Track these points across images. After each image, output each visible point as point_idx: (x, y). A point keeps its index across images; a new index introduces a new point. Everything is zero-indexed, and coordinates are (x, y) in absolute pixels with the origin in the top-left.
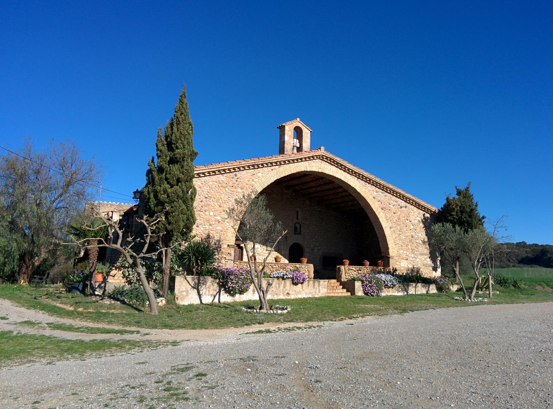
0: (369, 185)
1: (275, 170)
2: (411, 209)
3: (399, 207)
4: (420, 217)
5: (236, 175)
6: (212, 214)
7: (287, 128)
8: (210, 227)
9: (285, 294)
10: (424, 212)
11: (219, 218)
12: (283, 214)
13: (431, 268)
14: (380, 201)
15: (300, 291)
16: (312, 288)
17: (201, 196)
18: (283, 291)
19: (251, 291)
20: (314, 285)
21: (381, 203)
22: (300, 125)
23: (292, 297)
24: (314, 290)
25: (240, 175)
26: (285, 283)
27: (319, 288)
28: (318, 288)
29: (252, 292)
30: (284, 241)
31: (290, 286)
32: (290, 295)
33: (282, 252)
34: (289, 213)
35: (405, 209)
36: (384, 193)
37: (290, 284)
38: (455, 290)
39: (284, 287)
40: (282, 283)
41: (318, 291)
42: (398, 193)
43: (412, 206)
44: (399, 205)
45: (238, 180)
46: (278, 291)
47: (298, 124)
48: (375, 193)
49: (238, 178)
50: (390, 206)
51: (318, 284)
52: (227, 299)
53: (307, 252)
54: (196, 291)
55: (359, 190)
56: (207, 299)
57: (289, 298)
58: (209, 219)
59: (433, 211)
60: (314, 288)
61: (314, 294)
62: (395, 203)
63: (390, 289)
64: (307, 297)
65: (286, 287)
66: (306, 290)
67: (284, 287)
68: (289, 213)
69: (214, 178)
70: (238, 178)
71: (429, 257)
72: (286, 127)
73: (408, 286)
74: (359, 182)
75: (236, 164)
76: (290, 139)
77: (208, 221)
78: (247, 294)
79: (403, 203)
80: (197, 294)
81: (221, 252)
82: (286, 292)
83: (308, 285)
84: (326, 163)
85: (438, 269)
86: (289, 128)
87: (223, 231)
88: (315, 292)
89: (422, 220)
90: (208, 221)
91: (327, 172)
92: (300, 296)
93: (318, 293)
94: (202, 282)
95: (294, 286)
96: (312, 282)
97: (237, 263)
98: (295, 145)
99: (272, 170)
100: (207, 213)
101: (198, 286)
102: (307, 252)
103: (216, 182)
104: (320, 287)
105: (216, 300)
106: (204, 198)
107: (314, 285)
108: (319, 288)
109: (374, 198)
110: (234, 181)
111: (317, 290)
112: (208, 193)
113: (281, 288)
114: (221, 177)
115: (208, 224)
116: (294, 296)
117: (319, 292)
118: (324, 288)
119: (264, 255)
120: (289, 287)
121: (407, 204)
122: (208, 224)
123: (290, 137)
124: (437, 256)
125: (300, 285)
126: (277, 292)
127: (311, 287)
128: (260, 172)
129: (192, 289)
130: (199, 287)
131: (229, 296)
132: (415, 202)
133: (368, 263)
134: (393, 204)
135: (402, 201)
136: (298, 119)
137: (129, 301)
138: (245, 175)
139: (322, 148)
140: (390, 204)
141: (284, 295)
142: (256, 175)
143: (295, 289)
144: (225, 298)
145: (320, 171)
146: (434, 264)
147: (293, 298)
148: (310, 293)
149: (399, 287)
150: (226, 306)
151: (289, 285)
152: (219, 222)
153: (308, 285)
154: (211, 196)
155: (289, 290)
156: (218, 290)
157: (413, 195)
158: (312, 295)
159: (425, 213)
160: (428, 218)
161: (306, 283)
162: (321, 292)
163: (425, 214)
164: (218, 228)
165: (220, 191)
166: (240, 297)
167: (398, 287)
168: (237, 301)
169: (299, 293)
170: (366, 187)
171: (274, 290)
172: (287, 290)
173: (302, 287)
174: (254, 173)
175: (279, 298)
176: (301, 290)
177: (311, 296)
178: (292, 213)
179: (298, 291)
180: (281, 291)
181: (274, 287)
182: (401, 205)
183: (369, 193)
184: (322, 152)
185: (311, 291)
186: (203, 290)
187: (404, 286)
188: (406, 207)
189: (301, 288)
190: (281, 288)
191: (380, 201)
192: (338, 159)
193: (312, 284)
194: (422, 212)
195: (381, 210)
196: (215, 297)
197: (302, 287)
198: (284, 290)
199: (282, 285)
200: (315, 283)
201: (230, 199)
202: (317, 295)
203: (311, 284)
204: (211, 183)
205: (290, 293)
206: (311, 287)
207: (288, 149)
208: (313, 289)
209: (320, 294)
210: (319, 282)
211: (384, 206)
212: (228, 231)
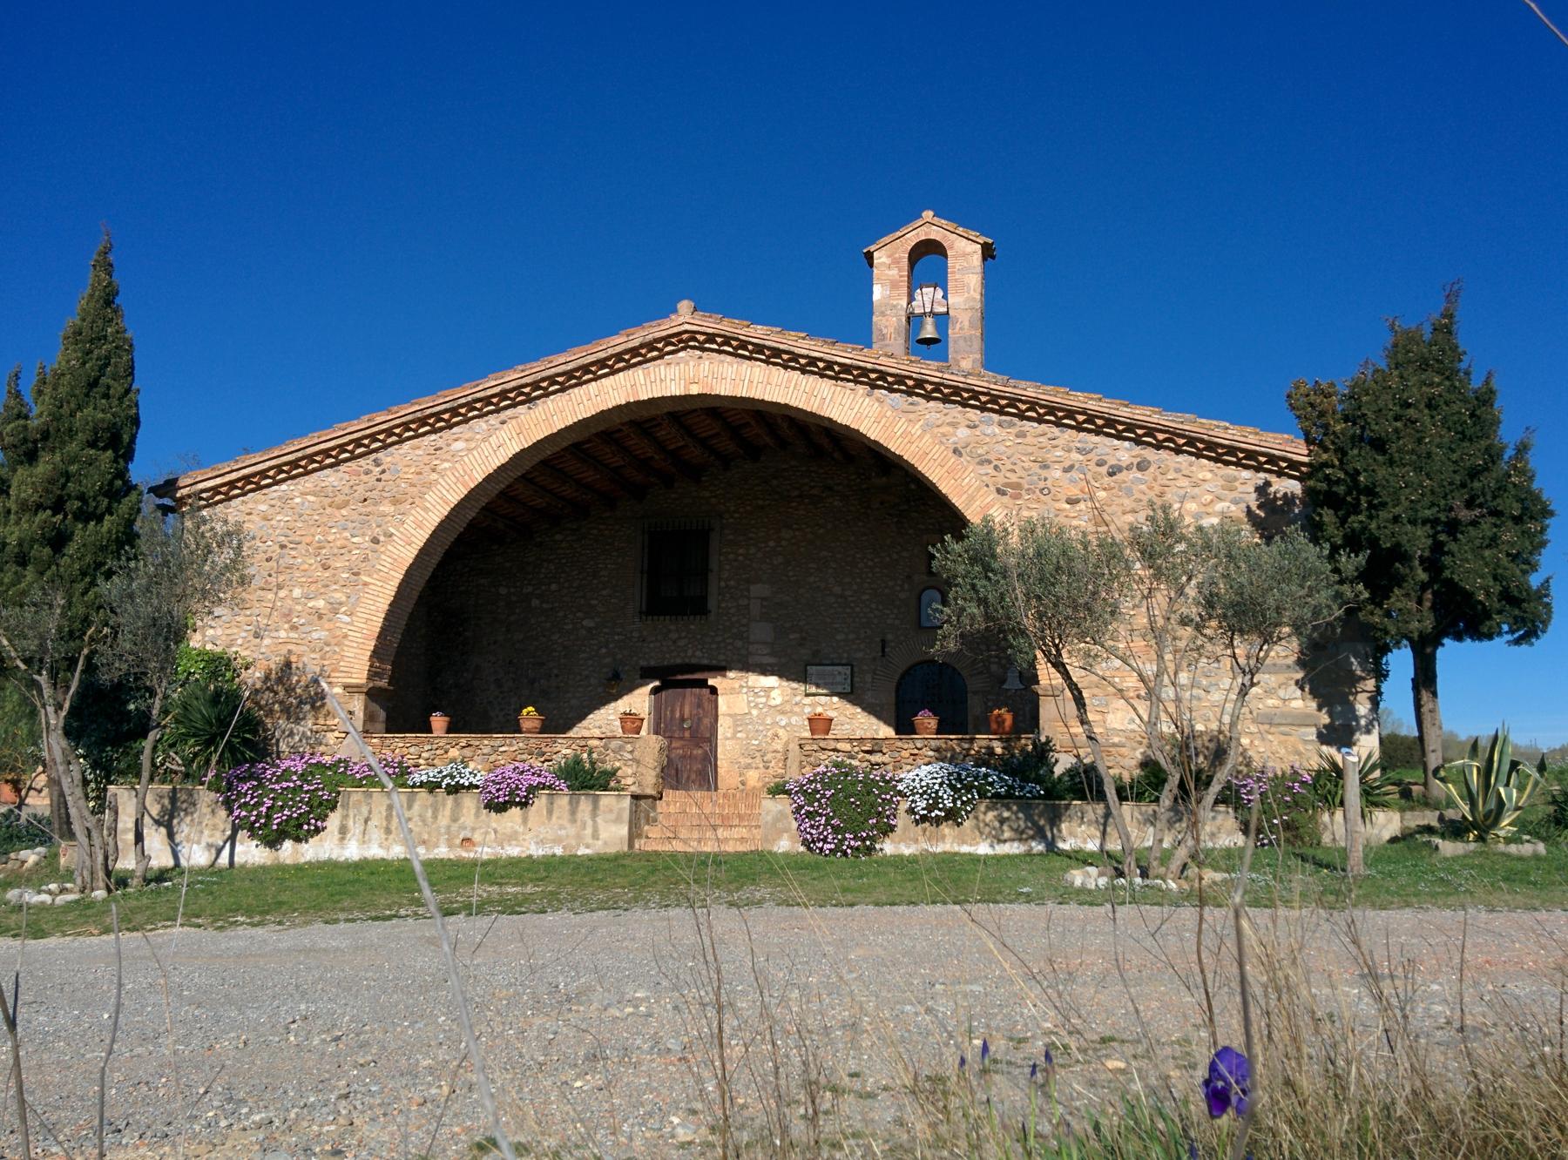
0: (932, 404)
1: (514, 421)
2: (1177, 470)
3: (1104, 470)
4: (1235, 502)
5: (377, 463)
6: (297, 592)
7: (880, 258)
8: (293, 635)
9: (458, 841)
10: (1262, 475)
11: (321, 603)
12: (870, 563)
13: (1311, 733)
14: (990, 462)
15: (516, 832)
16: (565, 822)
17: (270, 543)
18: (448, 832)
19: (332, 832)
20: (573, 812)
21: (996, 468)
22: (935, 234)
23: (485, 853)
24: (572, 830)
25: (389, 459)
26: (457, 804)
27: (595, 822)
28: (590, 823)
29: (337, 835)
30: (874, 659)
31: (477, 815)
32: (474, 845)
33: (869, 697)
34: (895, 556)
35: (1139, 475)
36: (1012, 425)
37: (478, 809)
38: (1387, 836)
39: (455, 819)
40: (444, 805)
41: (589, 831)
42: (1080, 413)
43: (1182, 458)
44: (1100, 464)
45: (384, 477)
46: (429, 833)
47: (926, 234)
48: (963, 433)
49: (383, 472)
50: (1044, 473)
51: (590, 808)
52: (254, 856)
53: (975, 693)
54: (163, 830)
55: (873, 433)
56: (197, 856)
57: (472, 855)
58: (290, 610)
59: (1303, 464)
60: (573, 821)
61: (574, 843)
62: (1075, 456)
63: (946, 829)
64: (541, 853)
65: (462, 820)
66: (542, 829)
67: (455, 819)
68: (895, 556)
69: (307, 483)
70: (383, 472)
71: (1300, 685)
72: (876, 255)
73: (1055, 818)
74: (878, 400)
75: (358, 426)
76: (895, 293)
77: (287, 615)
78: (321, 840)
79: (1125, 452)
80: (166, 838)
81: (324, 711)
82: (461, 837)
83: (550, 812)
84: (722, 357)
85: (1357, 736)
86: (889, 257)
87: (333, 641)
88: (579, 837)
89: (1249, 512)
90: (287, 615)
91: (724, 389)
92: (514, 851)
93: (590, 841)
94: (184, 806)
95: (493, 814)
96: (566, 799)
97: (374, 740)
98: (928, 310)
99: (503, 423)
100: (282, 594)
101: (172, 817)
102: (975, 693)
103: (314, 494)
104: (599, 820)
105: (224, 859)
106: (276, 547)
107: (573, 812)
108: (595, 822)
109: (955, 451)
110: (371, 479)
111: (584, 828)
112: (290, 533)
113: (444, 820)
114: (330, 478)
115: (286, 626)
116: (489, 850)
117: (595, 836)
118: (618, 820)
119: (796, 709)
120: (472, 817)
121: (1150, 454)
122: (286, 626)
123: (894, 285)
124: (1352, 672)
125: (515, 812)
126: (426, 837)
127: (559, 818)
128: (458, 440)
129: (155, 827)
130: (175, 821)
131: (261, 848)
132: (1183, 436)
133: (932, 723)
134: (1067, 464)
135: (1116, 442)
136: (928, 215)
137: (1156, 859)
138: (405, 457)
139: (685, 306)
140: (1046, 467)
141: (450, 846)
142: (445, 449)
143: (494, 825)
144: (250, 852)
145: (694, 390)
146: (1330, 714)
147: (485, 857)
148: (557, 841)
149: (1002, 821)
150: (257, 874)
151: (473, 811)
152: (320, 617)
153: (550, 812)
154: (297, 539)
155: (473, 829)
156: (229, 833)
157: (1167, 406)
158: (564, 848)
159: (1273, 478)
160: (1289, 499)
161: (540, 802)
162: (603, 835)
163: (1268, 484)
164: (315, 635)
165: (325, 520)
166: (296, 851)
167: (997, 824)
168: (288, 862)
169: (513, 837)
170: (911, 416)
171: (416, 829)
172: (465, 828)
173: (525, 820)
174: (440, 443)
175: (431, 856)
176: (521, 830)
177: (559, 851)
178: (905, 554)
179: (508, 831)
180: (443, 830)
181: (416, 819)
182: (1112, 462)
183: (927, 437)
184: (681, 320)
185: (563, 832)
186: (184, 829)
187: (1029, 818)
188: (1142, 466)
189: (519, 820)
190: (444, 820)
191: (990, 462)
192: (757, 333)
193: (567, 807)
194: (1246, 474)
195: (994, 495)
196: (219, 851)
197: (525, 820)
198: (455, 827)
199: (447, 812)
200: (578, 802)
201: (355, 540)
202: (588, 847)
203: (560, 807)
204: (298, 500)
205: (477, 837)
206: (559, 818)
207: (885, 331)
208: (568, 825)
209: (600, 842)
210: (596, 799)
211: (1014, 478)
212: (347, 643)
